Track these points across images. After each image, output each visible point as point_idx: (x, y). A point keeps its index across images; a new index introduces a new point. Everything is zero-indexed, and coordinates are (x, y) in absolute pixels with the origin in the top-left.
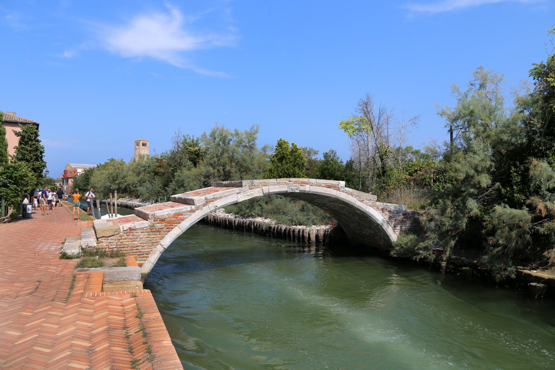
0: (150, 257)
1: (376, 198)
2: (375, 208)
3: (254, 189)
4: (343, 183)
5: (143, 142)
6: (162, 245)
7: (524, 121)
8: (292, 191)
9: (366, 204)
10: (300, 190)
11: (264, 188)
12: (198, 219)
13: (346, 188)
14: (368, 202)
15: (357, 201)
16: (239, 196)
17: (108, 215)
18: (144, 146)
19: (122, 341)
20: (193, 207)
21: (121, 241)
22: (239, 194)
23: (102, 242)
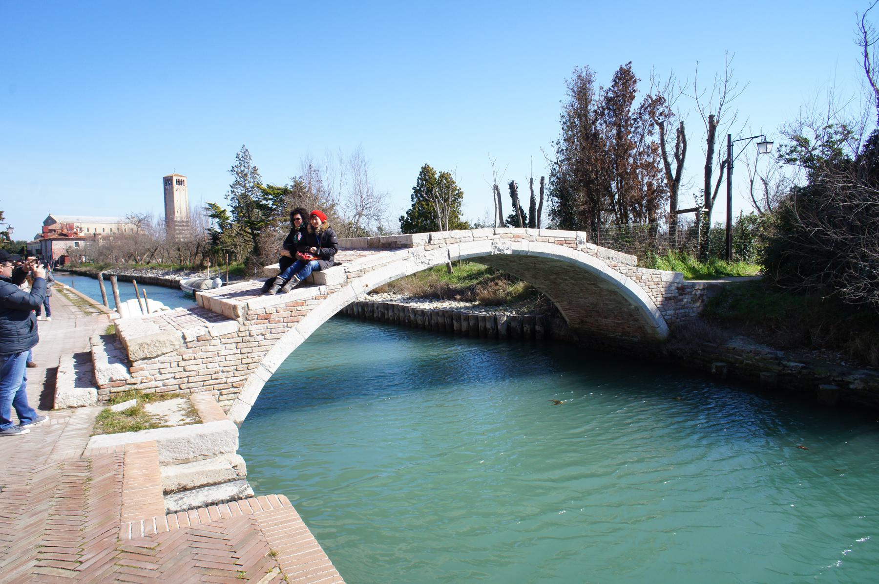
0: (242, 392)
1: (636, 261)
4: (583, 235)
5: (178, 178)
7: (372, 243)
8: (499, 253)
13: (587, 243)
18: (179, 184)
20: (323, 288)
23: (142, 369)
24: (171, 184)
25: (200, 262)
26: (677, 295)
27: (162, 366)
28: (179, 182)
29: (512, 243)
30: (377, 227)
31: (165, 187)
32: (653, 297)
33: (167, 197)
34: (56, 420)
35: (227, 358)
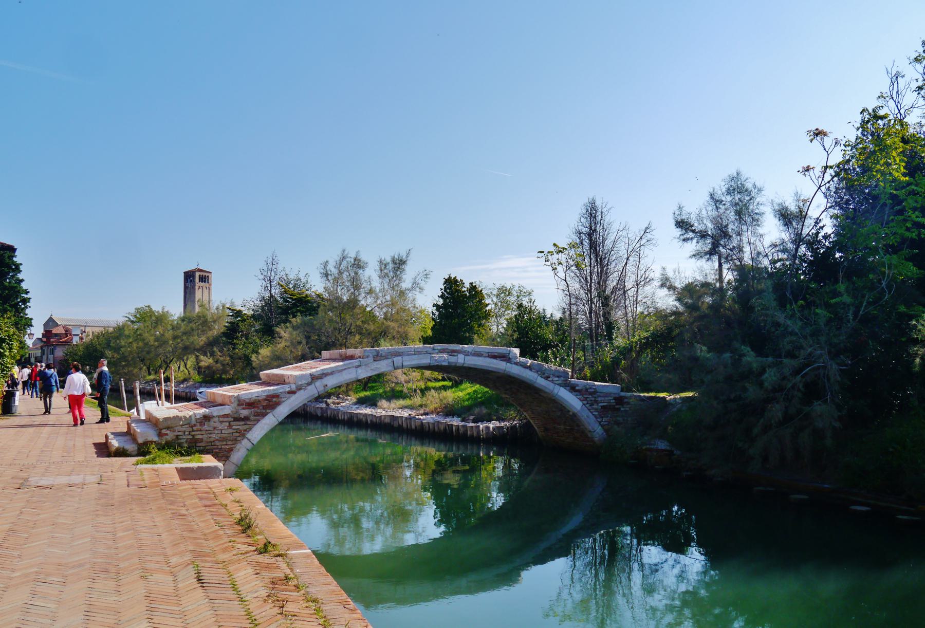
2: (568, 388)
3: (382, 362)
5: (201, 274)
6: (249, 440)
9: (552, 381)
10: (449, 363)
11: (395, 359)
12: (300, 403)
14: (557, 379)
15: (539, 378)
16: (359, 370)
17: (156, 402)
18: (202, 282)
19: (186, 609)
21: (193, 433)
22: (358, 369)
23: (167, 434)
24: (193, 281)
27: (179, 433)
28: (202, 278)
29: (449, 357)
31: (185, 285)
32: (588, 405)
33: (187, 296)
34: (82, 476)
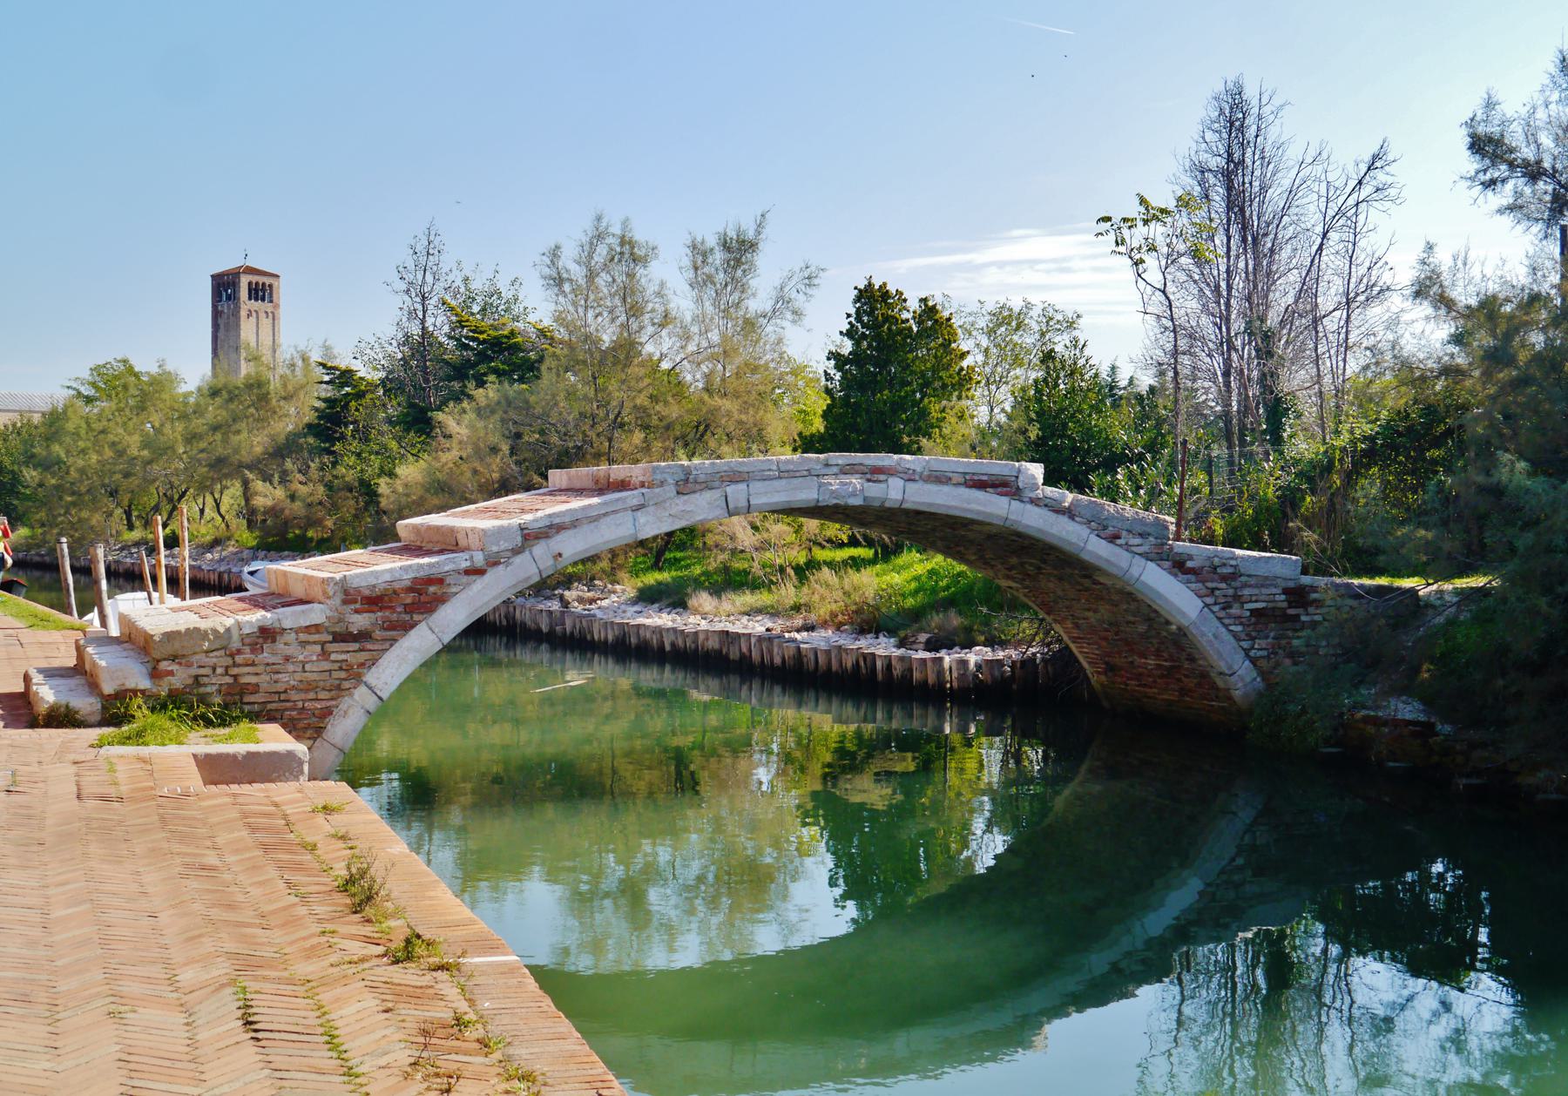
5: (254, 279)
18: (256, 299)
23: (171, 673)
24: (233, 297)
25: (1381, 565)
26: (1285, 605)
28: (256, 290)
29: (866, 485)
30: (924, 300)
31: (214, 307)
32: (1216, 608)
33: (221, 334)
35: (308, 667)
